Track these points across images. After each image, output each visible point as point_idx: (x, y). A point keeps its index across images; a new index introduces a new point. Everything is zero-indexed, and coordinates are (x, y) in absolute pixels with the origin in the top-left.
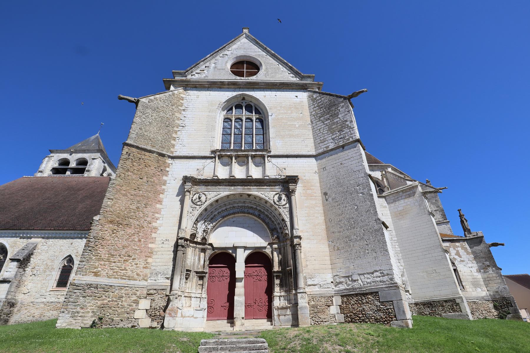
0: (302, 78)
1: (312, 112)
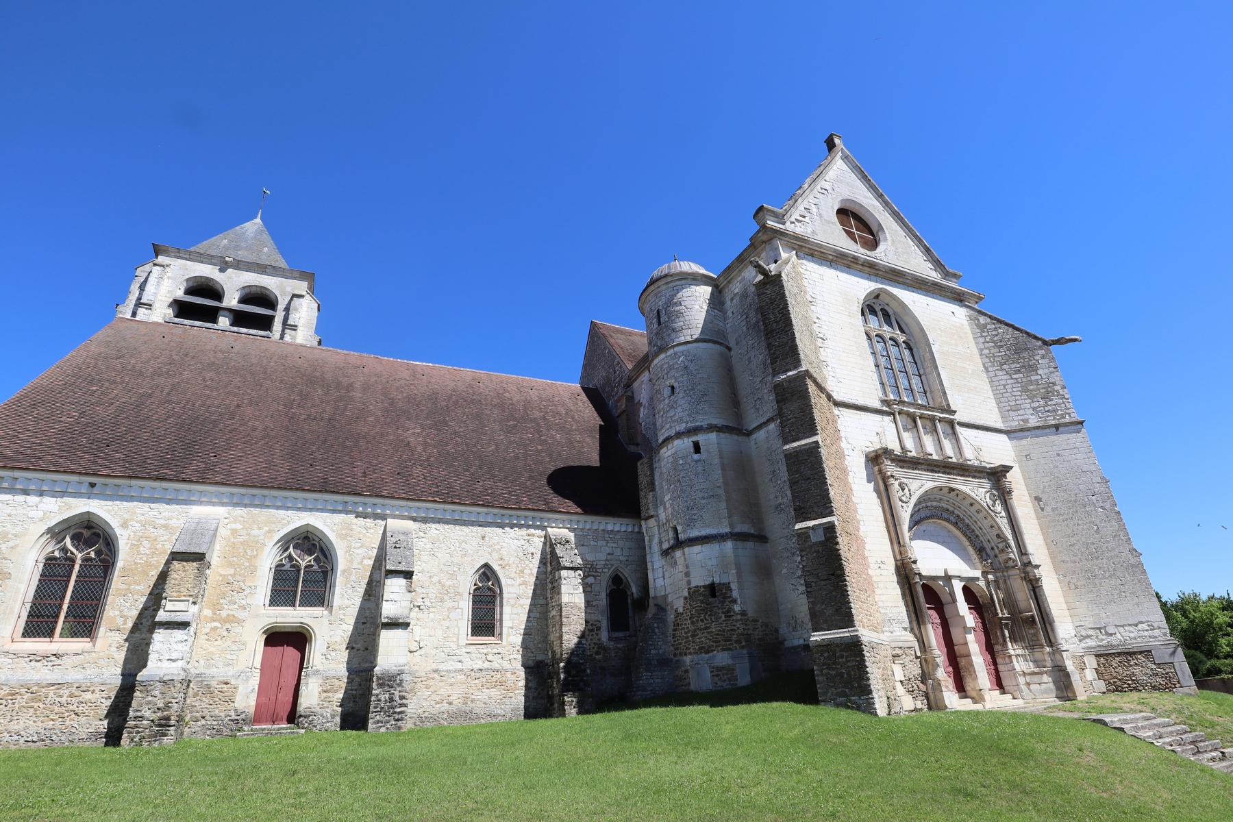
0: (947, 274)
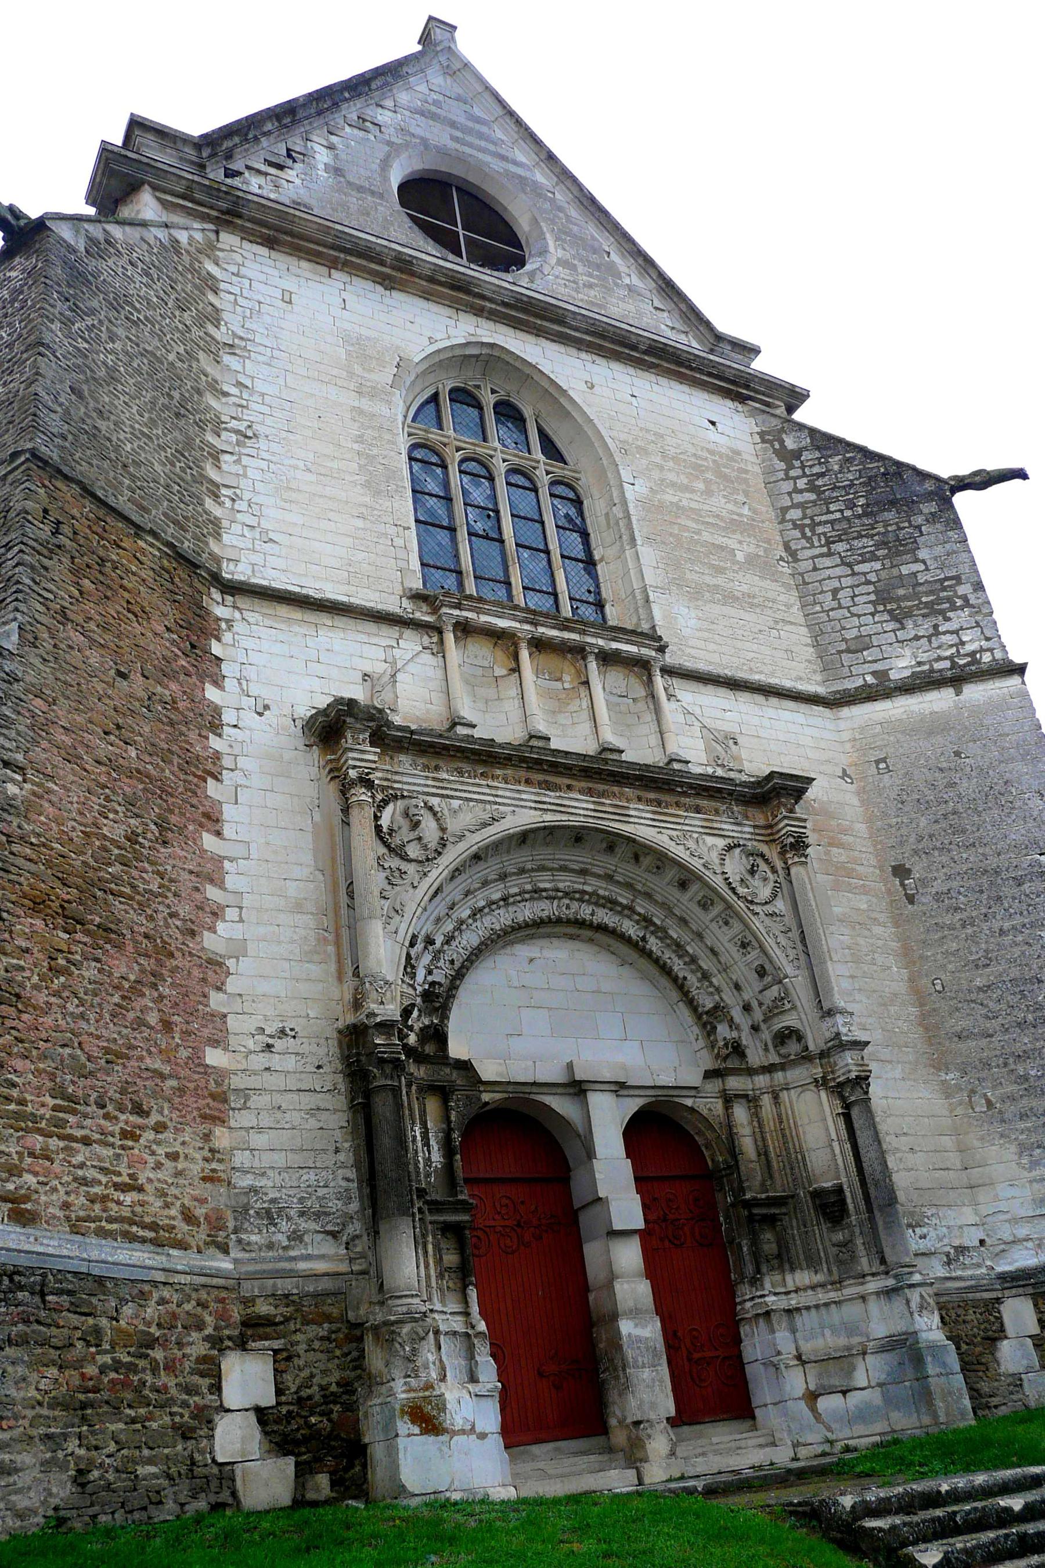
1: (784, 510)
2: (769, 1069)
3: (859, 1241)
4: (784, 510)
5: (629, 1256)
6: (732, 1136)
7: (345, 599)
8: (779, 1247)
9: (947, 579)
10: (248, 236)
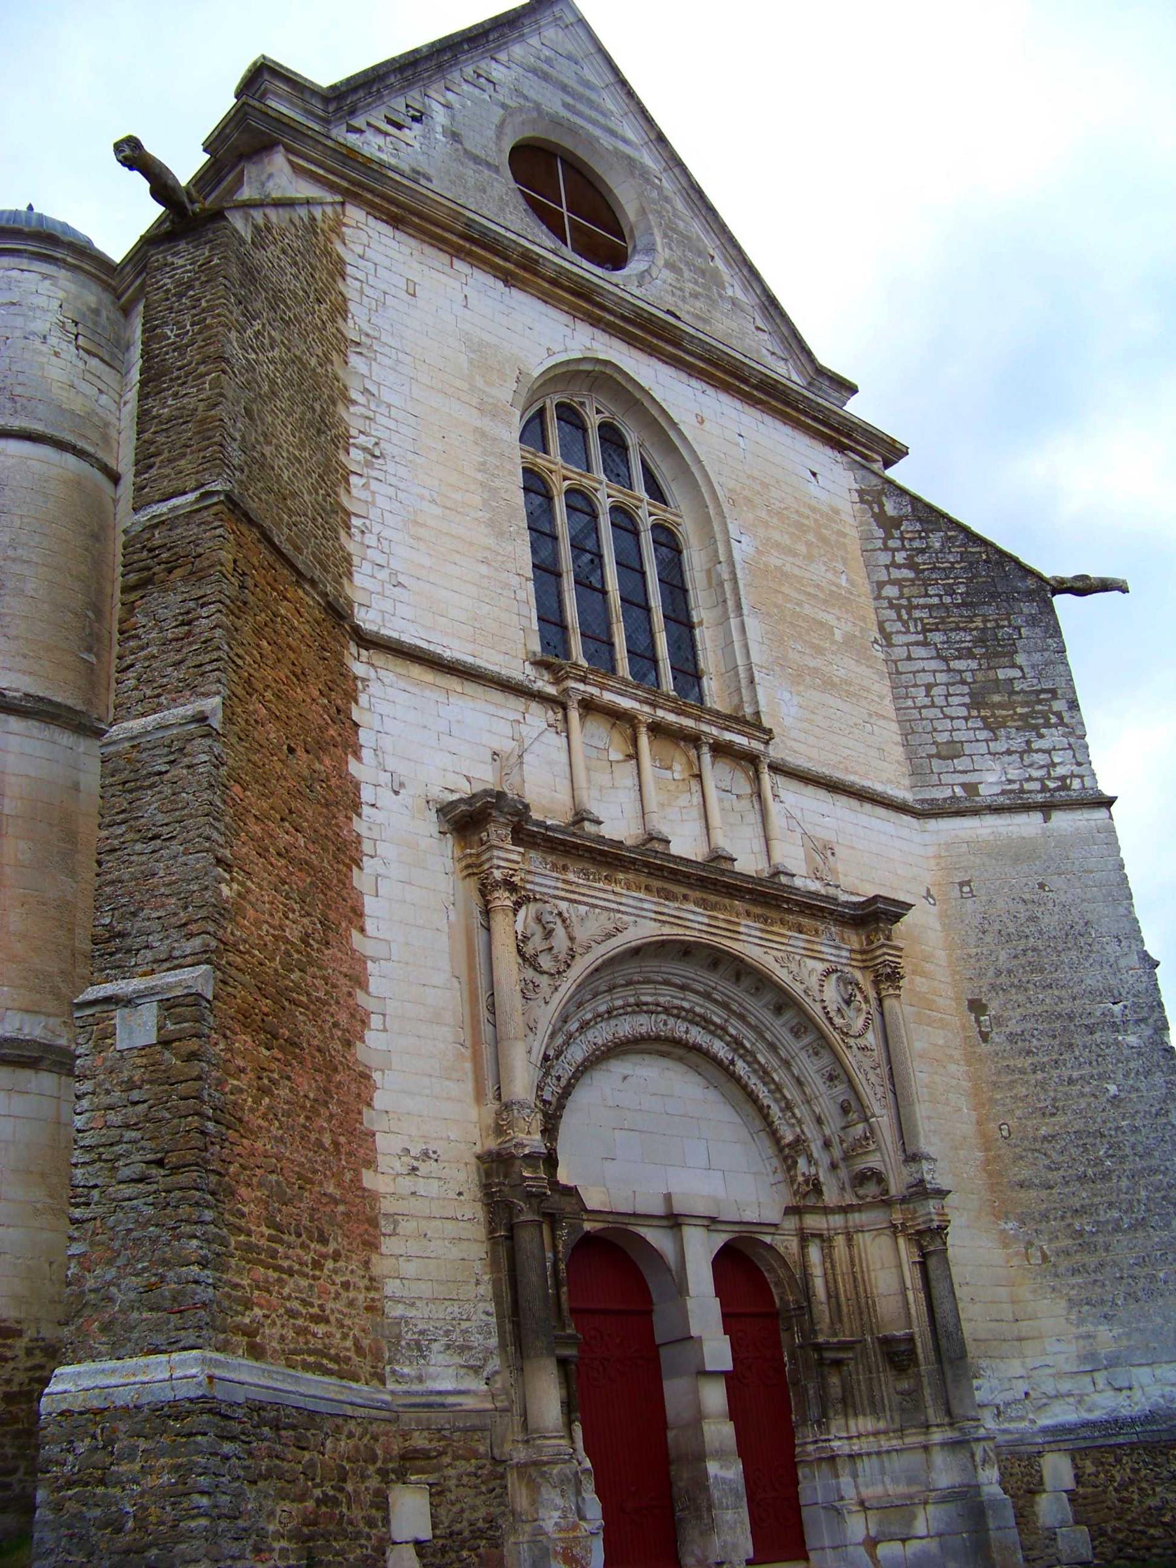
1: (880, 585)
2: (845, 1210)
3: (927, 1391)
4: (880, 585)
5: (715, 1397)
6: (807, 1276)
7: (470, 660)
8: (844, 1391)
9: (1043, 691)
10: (375, 211)
